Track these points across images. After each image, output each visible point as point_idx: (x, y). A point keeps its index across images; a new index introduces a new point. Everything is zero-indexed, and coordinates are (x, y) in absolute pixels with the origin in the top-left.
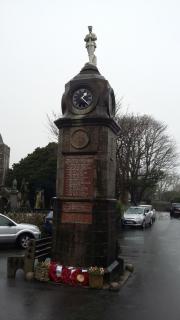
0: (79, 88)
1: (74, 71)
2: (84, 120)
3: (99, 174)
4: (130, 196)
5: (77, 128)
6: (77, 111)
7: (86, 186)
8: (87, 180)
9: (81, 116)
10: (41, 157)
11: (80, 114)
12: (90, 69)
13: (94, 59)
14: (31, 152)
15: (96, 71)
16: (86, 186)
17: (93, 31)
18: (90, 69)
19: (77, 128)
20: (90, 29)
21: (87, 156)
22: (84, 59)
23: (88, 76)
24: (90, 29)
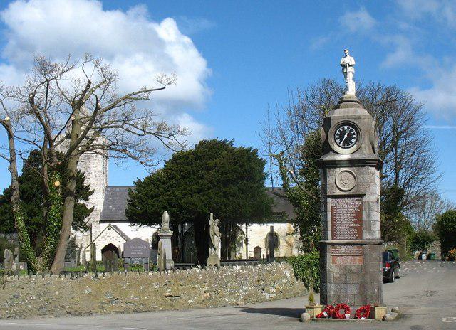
7: (355, 228)
8: (355, 222)
16: (355, 228)
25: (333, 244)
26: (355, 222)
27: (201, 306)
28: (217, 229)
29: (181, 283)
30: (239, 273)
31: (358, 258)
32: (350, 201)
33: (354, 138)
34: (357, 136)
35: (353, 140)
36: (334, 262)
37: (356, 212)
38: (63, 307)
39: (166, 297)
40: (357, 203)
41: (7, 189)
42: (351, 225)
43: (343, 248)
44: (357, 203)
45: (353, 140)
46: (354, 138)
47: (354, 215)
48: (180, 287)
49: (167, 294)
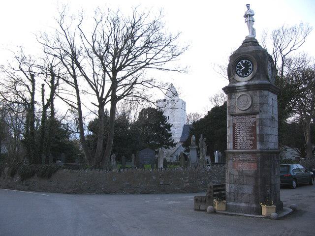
0: (241, 59)
1: (236, 44)
2: (248, 87)
3: (104, 150)
4: (59, 161)
5: (243, 93)
6: (239, 79)
7: (251, 140)
8: (250, 136)
9: (243, 84)
10: (217, 115)
11: (243, 82)
12: (251, 42)
13: (253, 31)
14: (210, 110)
15: (255, 43)
16: (251, 140)
17: (251, 8)
18: (251, 42)
19: (243, 93)
20: (248, 6)
21: (251, 116)
22: (245, 33)
23: (252, 48)
24: (248, 6)
25: (233, 153)
26: (250, 136)
27: (183, 191)
28: (204, 143)
29: (171, 176)
30: (210, 171)
31: (253, 164)
32: (247, 118)
33: (250, 69)
34: (253, 67)
35: (250, 71)
36: (234, 167)
37: (252, 128)
38: (101, 188)
39: (161, 185)
40: (252, 120)
41: (92, 121)
42: (248, 137)
43: (241, 156)
44: (252, 120)
45: (250, 71)
46: (250, 69)
47: (250, 130)
48: (170, 179)
49: (161, 183)
